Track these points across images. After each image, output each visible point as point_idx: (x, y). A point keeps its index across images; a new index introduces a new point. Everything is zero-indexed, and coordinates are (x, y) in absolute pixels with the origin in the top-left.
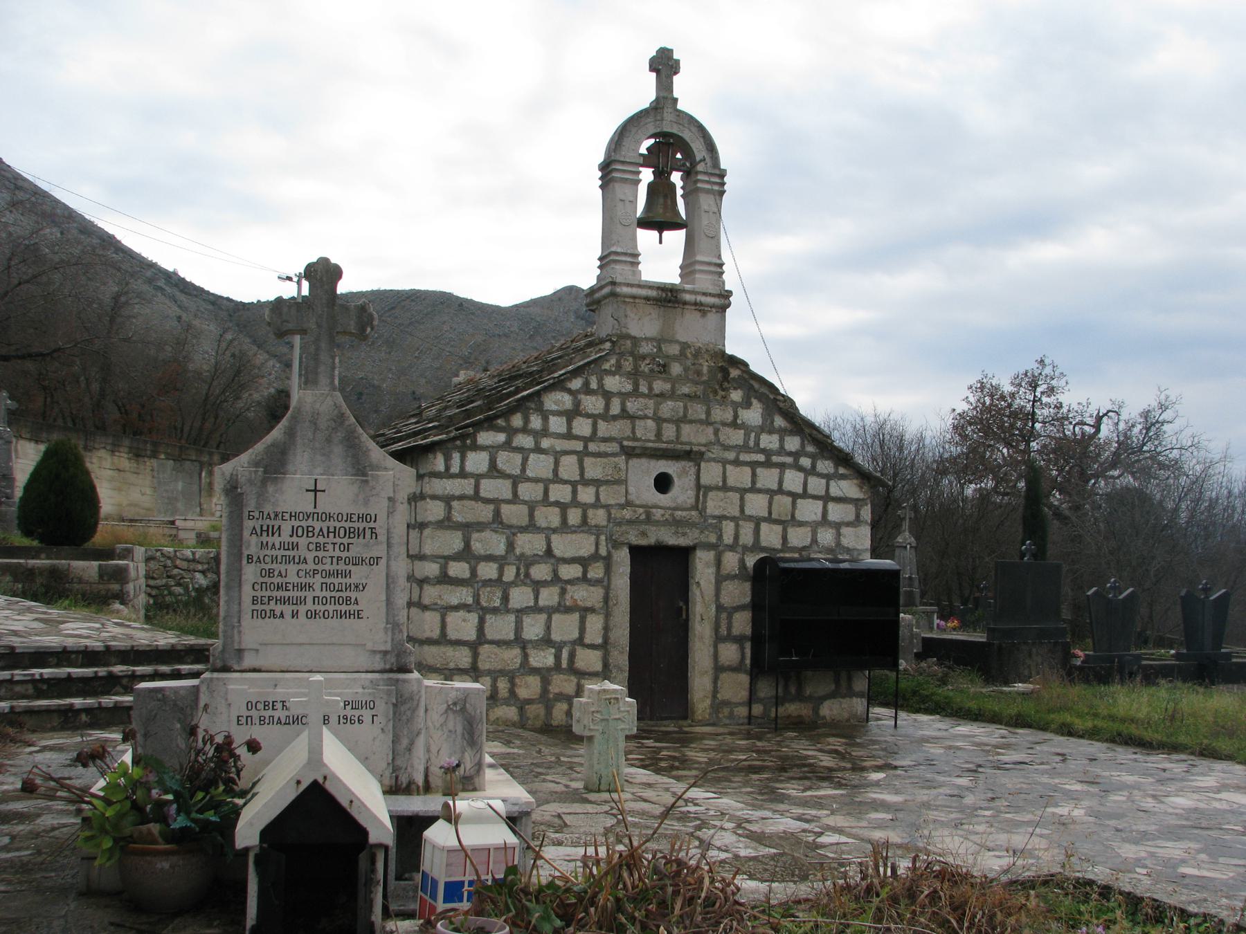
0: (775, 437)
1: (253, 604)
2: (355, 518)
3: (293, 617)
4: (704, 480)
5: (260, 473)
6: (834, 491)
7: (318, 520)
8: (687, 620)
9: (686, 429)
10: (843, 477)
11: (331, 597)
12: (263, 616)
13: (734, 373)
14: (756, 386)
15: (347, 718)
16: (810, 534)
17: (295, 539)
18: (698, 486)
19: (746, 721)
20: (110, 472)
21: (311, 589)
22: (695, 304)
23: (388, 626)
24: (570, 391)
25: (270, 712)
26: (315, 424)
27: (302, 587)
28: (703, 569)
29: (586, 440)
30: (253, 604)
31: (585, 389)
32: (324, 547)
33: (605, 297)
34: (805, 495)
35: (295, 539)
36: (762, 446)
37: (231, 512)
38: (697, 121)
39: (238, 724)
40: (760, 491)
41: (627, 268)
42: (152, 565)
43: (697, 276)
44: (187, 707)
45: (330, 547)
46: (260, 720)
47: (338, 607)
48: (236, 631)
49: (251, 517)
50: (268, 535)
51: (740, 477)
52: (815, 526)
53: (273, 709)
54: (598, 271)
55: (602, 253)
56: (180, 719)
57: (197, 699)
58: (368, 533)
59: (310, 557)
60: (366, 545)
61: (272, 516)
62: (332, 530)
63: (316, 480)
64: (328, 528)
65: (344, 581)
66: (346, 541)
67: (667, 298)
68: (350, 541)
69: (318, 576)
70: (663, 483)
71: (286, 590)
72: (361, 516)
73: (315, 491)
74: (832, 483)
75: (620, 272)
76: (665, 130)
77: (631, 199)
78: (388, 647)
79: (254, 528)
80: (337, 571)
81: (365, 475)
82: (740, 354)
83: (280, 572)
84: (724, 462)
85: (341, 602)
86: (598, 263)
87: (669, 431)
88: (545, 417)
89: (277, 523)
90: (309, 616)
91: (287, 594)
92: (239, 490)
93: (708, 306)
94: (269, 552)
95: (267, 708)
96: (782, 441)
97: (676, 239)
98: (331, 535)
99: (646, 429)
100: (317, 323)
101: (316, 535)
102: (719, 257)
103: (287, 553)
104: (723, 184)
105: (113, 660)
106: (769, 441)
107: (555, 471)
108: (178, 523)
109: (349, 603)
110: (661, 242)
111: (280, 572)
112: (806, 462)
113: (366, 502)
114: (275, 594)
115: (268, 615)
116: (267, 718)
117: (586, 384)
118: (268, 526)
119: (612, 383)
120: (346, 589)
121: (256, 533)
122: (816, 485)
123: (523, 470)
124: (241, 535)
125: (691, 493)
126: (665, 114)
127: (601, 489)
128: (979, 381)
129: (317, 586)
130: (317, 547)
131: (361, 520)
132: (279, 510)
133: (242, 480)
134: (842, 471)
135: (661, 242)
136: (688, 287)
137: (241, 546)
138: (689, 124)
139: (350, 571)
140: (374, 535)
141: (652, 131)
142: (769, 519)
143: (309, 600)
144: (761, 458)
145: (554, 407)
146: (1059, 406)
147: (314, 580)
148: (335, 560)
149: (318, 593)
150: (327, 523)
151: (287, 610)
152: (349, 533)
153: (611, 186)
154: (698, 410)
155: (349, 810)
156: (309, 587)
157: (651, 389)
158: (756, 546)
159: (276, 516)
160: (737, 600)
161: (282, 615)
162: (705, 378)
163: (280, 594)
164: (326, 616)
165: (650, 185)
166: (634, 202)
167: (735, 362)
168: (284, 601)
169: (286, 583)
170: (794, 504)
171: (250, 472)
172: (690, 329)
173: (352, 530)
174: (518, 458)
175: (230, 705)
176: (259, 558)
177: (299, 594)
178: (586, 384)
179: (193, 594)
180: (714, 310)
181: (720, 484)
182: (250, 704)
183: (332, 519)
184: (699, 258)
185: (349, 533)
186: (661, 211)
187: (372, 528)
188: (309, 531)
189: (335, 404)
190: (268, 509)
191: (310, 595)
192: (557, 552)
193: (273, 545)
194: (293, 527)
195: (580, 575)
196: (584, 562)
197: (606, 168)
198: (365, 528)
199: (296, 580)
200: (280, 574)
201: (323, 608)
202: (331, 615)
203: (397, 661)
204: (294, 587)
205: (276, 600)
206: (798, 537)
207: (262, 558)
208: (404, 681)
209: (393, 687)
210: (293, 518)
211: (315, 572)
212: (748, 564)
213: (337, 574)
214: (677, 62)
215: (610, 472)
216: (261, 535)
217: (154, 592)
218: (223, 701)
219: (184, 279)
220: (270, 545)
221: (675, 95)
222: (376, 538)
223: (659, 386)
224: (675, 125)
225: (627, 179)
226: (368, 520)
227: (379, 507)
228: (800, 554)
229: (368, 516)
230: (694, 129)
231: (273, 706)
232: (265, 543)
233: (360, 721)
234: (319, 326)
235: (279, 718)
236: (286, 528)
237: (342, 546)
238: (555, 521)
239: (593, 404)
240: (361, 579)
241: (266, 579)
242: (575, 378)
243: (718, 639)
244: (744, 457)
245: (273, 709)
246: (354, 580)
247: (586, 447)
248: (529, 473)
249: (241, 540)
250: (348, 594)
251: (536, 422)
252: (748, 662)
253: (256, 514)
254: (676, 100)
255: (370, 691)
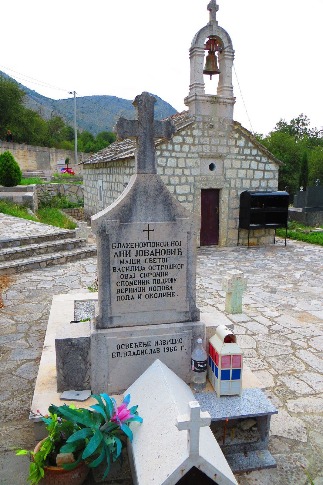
0: (249, 150)
1: (117, 293)
2: (170, 244)
3: (138, 298)
4: (225, 166)
5: (118, 222)
6: (267, 168)
7: (150, 247)
8: (219, 213)
9: (220, 148)
10: (270, 163)
11: (158, 287)
12: (123, 299)
13: (236, 127)
14: (243, 132)
15: (168, 349)
16: (259, 183)
17: (138, 257)
18: (223, 168)
19: (237, 245)
20: (22, 156)
21: (148, 283)
22: (224, 102)
23: (188, 299)
24: (181, 136)
25: (129, 349)
26: (147, 193)
27: (143, 283)
28: (224, 197)
29: (187, 153)
30: (117, 293)
31: (186, 134)
32: (154, 260)
33: (192, 101)
34: (258, 170)
35: (138, 257)
36: (244, 153)
37: (103, 245)
38: (225, 30)
39: (113, 357)
40: (243, 169)
41: (200, 89)
42: (39, 189)
43: (224, 92)
44: (85, 348)
45: (157, 260)
46: (124, 354)
47: (162, 291)
48: (109, 308)
49: (114, 247)
50: (124, 256)
51: (237, 164)
52: (260, 180)
53: (131, 348)
54: (189, 91)
55: (191, 84)
56: (81, 354)
57: (89, 344)
58: (177, 251)
59: (147, 266)
60: (176, 258)
61: (126, 246)
62: (158, 251)
63: (149, 225)
64: (156, 250)
65: (165, 278)
66: (165, 257)
67: (214, 100)
68: (168, 256)
69: (151, 276)
70: (212, 167)
71: (134, 285)
72: (173, 243)
73: (148, 231)
74: (267, 165)
75: (198, 91)
76: (214, 34)
77: (202, 62)
78: (188, 310)
79: (116, 253)
80: (161, 273)
81: (174, 220)
82: (239, 121)
83: (131, 275)
84: (232, 159)
85: (163, 289)
86: (189, 88)
87: (214, 149)
88: (173, 144)
89: (128, 250)
90: (147, 297)
91: (135, 287)
92: (107, 232)
93: (228, 103)
94: (125, 265)
95: (127, 347)
96: (251, 151)
97: (216, 77)
98: (158, 254)
99: (207, 149)
100: (144, 132)
101: (149, 254)
102: (232, 84)
103: (135, 265)
104: (234, 56)
105: (32, 242)
106: (247, 151)
107: (177, 164)
108: (44, 172)
109: (167, 289)
110: (211, 79)
111: (131, 275)
112: (258, 158)
113: (176, 235)
114: (129, 287)
115: (125, 298)
116: (128, 352)
117: (187, 133)
118: (124, 251)
119: (195, 132)
120: (166, 282)
121: (117, 256)
122: (261, 166)
123: (166, 164)
124: (109, 257)
125: (221, 170)
126: (213, 28)
127: (192, 170)
128: (279, 122)
129: (151, 282)
130: (150, 261)
131: (173, 245)
132: (129, 242)
133: (108, 227)
134: (270, 161)
135: (211, 79)
136: (221, 96)
137: (109, 263)
138: (222, 31)
139: (168, 272)
140: (180, 252)
141: (209, 35)
142: (246, 179)
143: (147, 289)
144: (244, 157)
145: (176, 142)
146: (306, 129)
147: (149, 279)
148: (160, 267)
149: (151, 285)
150: (155, 248)
151: (136, 295)
152: (166, 252)
153: (194, 58)
154: (224, 142)
155: (214, 480)
156: (147, 282)
157: (208, 134)
158: (242, 188)
159: (128, 245)
160: (235, 206)
161: (133, 298)
162: (226, 130)
163: (131, 287)
164: (156, 296)
165: (207, 57)
166: (202, 64)
167: (236, 123)
168: (134, 290)
169: (134, 281)
170: (254, 173)
171: (112, 222)
172: (222, 111)
173: (168, 251)
174: (165, 160)
175: (108, 347)
176: (119, 269)
177: (141, 286)
178: (187, 133)
179: (52, 198)
180: (230, 105)
181: (231, 167)
182: (118, 346)
183: (158, 245)
184: (225, 85)
185: (166, 252)
186: (212, 67)
187: (179, 249)
188: (145, 253)
189: (157, 181)
190: (123, 242)
191: (147, 286)
192: (178, 192)
193: (127, 261)
194: (137, 251)
195: (185, 199)
196: (186, 195)
197: (192, 50)
198: (175, 249)
199: (139, 279)
200: (131, 277)
201: (154, 292)
202: (158, 296)
203: (192, 315)
204: (138, 282)
205: (130, 290)
206: (255, 184)
207: (121, 269)
208: (197, 327)
209: (191, 331)
210: (137, 246)
211: (150, 274)
212: (239, 194)
213: (161, 274)
214: (218, 6)
215: (195, 164)
216: (120, 256)
217: (40, 198)
218: (104, 346)
219: (37, 93)
220: (125, 262)
221: (217, 20)
222: (181, 254)
223: (211, 132)
224: (217, 32)
225: (200, 55)
226: (177, 245)
227: (182, 237)
228: (255, 190)
229: (177, 243)
230: (224, 34)
231: (131, 346)
232: (122, 261)
233: (175, 350)
234: (145, 134)
235: (134, 352)
236: (134, 251)
237: (163, 259)
238: (177, 181)
239: (189, 140)
240: (173, 276)
241: (124, 280)
242: (183, 131)
243: (229, 219)
244: (239, 157)
245: (131, 348)
246: (170, 276)
247: (187, 155)
248: (168, 165)
249: (109, 260)
250: (167, 284)
251: (170, 147)
252: (238, 226)
253: (117, 245)
254: (217, 22)
255: (180, 333)
